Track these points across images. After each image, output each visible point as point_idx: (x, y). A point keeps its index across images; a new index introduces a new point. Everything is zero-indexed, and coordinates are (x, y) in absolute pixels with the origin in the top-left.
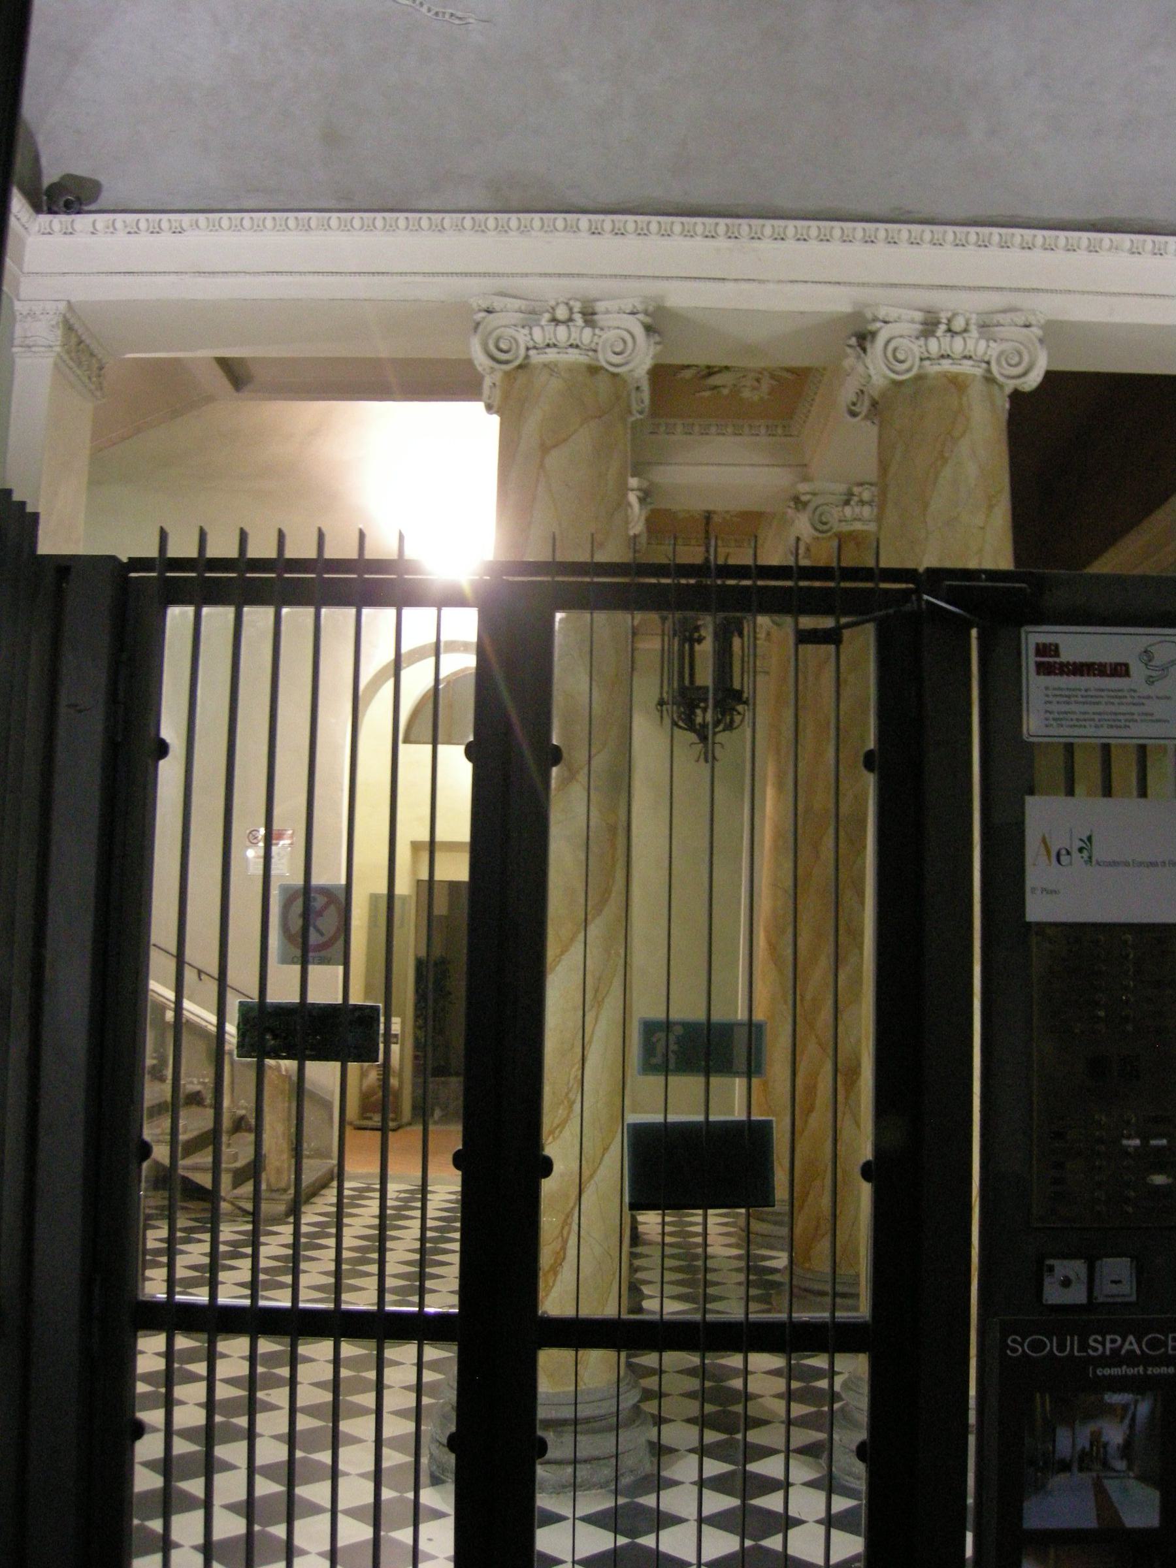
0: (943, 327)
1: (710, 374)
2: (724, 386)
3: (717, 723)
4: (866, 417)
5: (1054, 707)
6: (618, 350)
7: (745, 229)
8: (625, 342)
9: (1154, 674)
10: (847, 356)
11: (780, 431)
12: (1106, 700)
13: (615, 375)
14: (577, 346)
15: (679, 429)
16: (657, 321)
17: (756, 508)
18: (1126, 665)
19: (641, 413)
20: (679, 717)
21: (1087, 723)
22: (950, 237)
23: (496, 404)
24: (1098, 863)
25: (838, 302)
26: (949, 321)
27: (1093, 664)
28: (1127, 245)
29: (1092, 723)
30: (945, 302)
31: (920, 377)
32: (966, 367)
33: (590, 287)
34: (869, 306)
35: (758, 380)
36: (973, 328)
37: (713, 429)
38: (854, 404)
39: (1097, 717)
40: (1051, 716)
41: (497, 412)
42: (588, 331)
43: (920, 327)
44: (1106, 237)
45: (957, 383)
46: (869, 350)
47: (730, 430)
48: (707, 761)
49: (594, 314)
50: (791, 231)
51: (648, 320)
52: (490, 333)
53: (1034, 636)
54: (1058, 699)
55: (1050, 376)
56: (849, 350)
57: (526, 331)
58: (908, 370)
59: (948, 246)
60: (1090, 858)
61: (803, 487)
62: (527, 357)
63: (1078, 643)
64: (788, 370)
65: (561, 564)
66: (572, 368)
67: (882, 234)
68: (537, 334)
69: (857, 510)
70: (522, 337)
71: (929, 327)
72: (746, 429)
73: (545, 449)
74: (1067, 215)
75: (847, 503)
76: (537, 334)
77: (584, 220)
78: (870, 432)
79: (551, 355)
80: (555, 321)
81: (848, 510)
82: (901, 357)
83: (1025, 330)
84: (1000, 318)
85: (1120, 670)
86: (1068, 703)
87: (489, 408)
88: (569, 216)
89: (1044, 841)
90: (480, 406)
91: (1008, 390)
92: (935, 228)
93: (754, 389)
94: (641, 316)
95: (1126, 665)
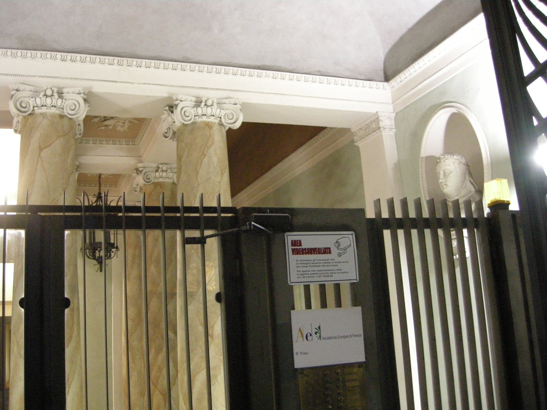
0: (203, 104)
1: (105, 120)
2: (110, 125)
3: (106, 256)
4: (171, 138)
5: (301, 269)
6: (72, 108)
7: (125, 62)
8: (75, 105)
9: (341, 252)
10: (164, 114)
11: (131, 143)
12: (321, 265)
13: (71, 119)
14: (55, 107)
15: (91, 141)
16: (89, 98)
17: (119, 173)
18: (329, 248)
19: (80, 135)
20: (90, 255)
21: (315, 275)
22: (206, 69)
23: (19, 130)
24: (324, 339)
25: (162, 93)
26: (206, 101)
27: (315, 249)
28: (272, 75)
29: (317, 275)
30: (204, 94)
31: (194, 123)
32: (212, 119)
33: (60, 83)
34: (174, 94)
35: (124, 123)
36: (215, 104)
37: (104, 142)
38: (166, 133)
39: (319, 272)
40: (300, 273)
41: (20, 133)
42: (60, 101)
43: (194, 103)
44: (264, 72)
45: (209, 126)
46: (174, 112)
47: (111, 142)
48: (101, 271)
49: (62, 93)
50: (144, 64)
51: (85, 97)
52: (18, 100)
53: (290, 237)
54: (303, 265)
55: (243, 123)
56: (165, 112)
57: (33, 99)
58: (190, 120)
59: (205, 73)
60: (320, 336)
61: (140, 165)
62: (33, 110)
63: (309, 240)
64: (134, 119)
65: (67, 207)
66: (53, 116)
67: (179, 67)
68: (38, 101)
69: (161, 174)
70: (32, 102)
71: (198, 103)
72: (118, 142)
73: (41, 149)
74: (248, 63)
75: (157, 171)
76: (38, 101)
77: (59, 55)
78: (172, 145)
79: (44, 110)
80: (46, 95)
81: (157, 174)
82: (187, 115)
83: (234, 106)
84: (225, 101)
85: (327, 251)
86: (306, 267)
87: (16, 131)
88: (53, 53)
89: (300, 330)
90: (12, 131)
91: (227, 128)
92: (200, 65)
93: (122, 126)
94: (82, 95)
95: (329, 248)
